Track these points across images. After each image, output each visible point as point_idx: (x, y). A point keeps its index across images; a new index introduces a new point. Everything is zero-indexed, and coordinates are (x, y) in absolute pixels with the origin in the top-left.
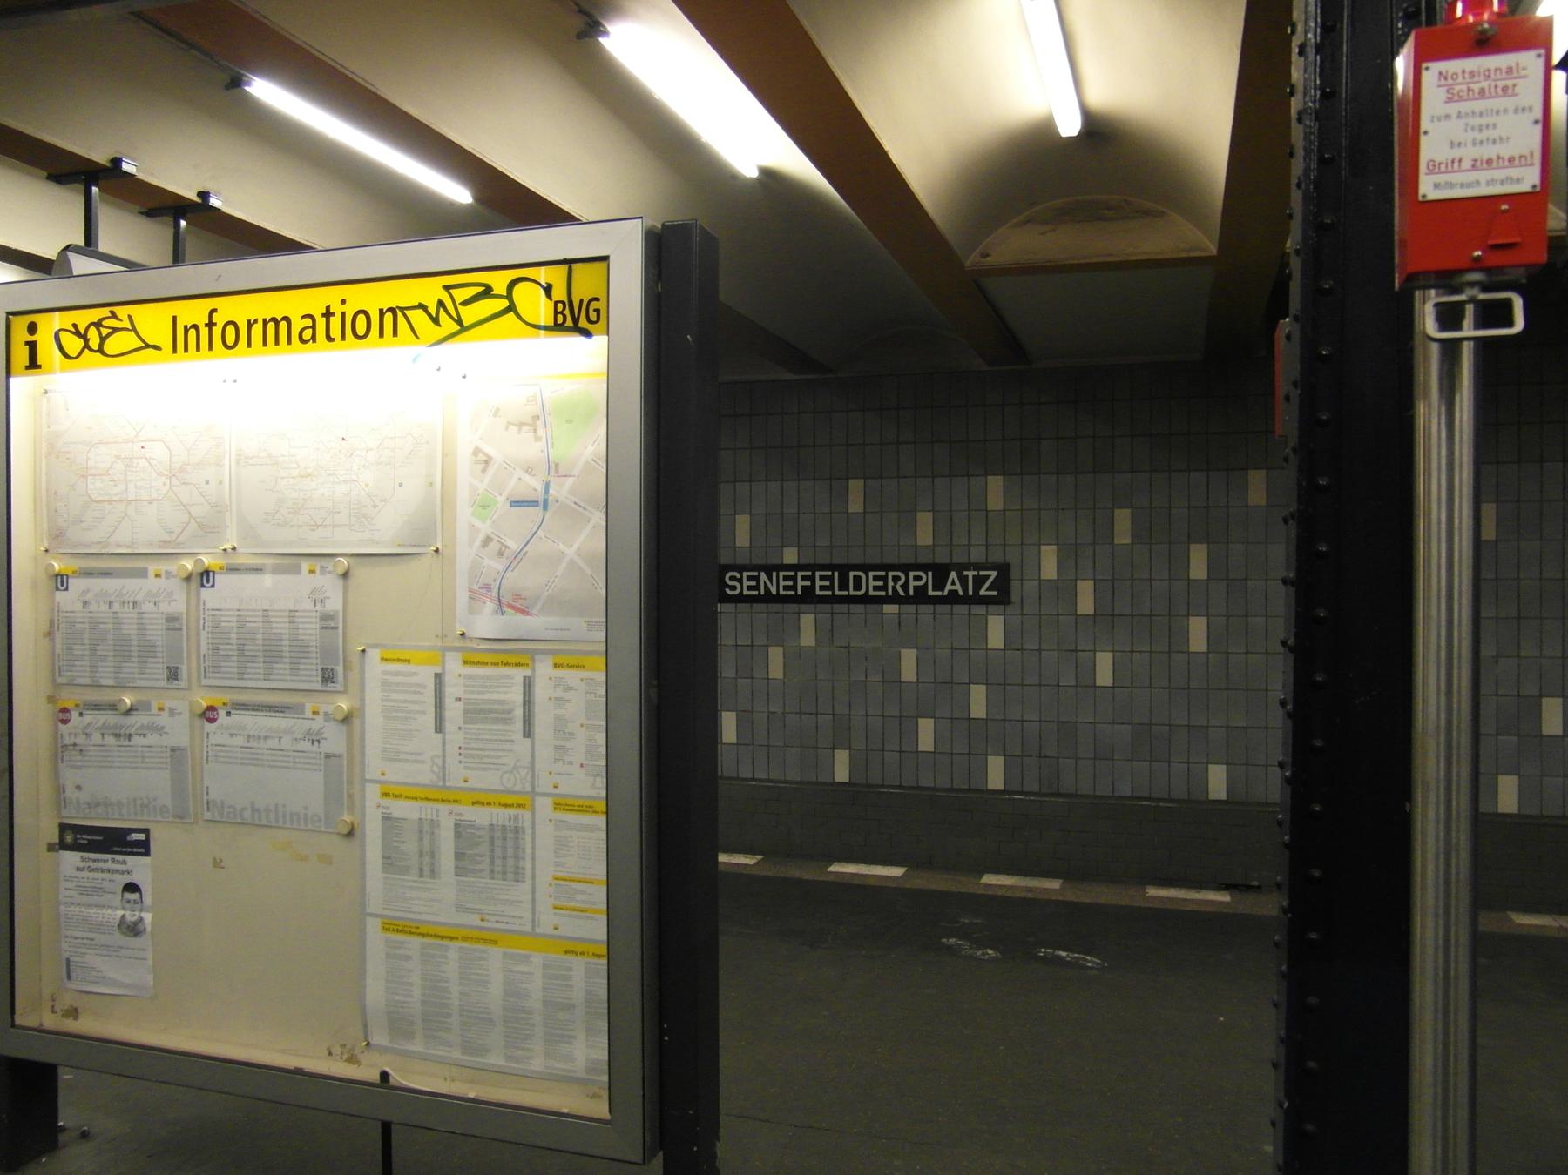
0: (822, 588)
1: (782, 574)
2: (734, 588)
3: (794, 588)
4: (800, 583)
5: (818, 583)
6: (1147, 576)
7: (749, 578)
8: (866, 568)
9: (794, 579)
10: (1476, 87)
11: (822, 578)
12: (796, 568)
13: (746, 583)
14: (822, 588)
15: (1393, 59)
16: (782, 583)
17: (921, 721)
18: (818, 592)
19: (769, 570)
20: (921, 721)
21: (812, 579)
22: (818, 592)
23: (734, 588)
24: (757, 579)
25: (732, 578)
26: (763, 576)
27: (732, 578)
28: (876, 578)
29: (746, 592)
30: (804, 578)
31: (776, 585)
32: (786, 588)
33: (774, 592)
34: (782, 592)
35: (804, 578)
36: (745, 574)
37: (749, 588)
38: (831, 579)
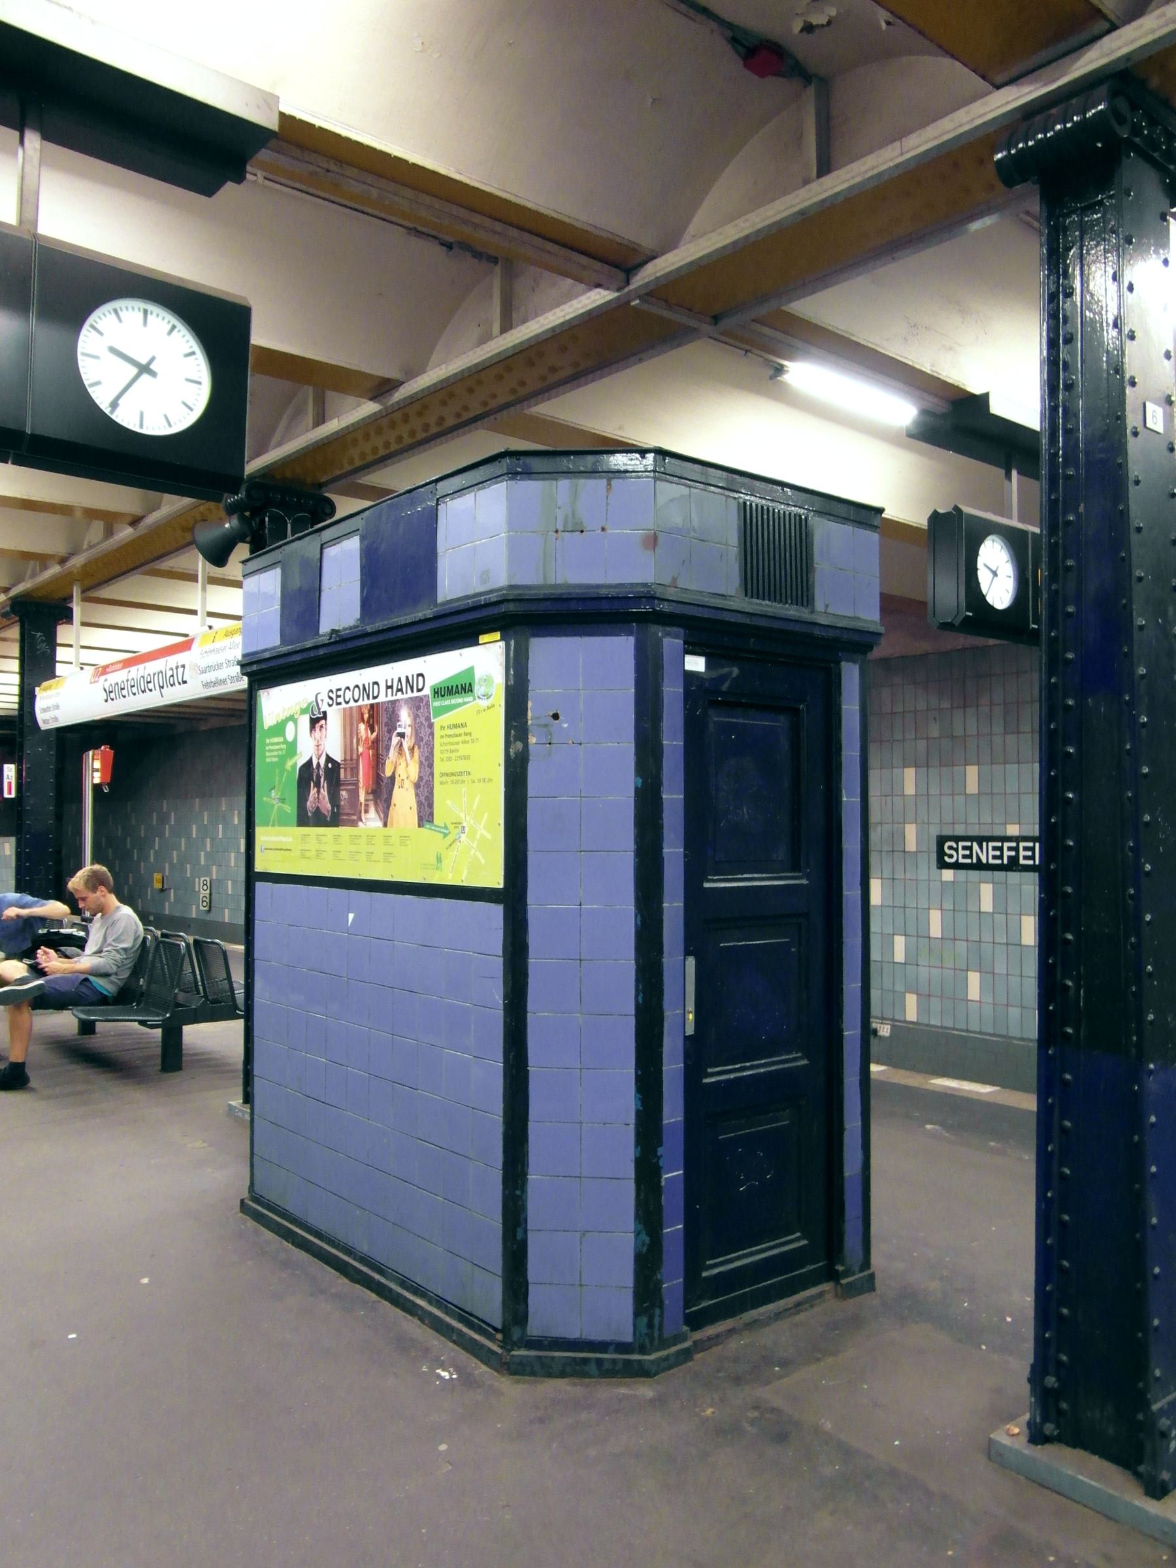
0: (1025, 858)
1: (991, 844)
2: (951, 856)
3: (1001, 857)
4: (1006, 853)
5: (1022, 853)
6: (1024, 887)
7: (964, 848)
8: (957, 839)
9: (1001, 849)
10: (431, 419)
11: (1025, 849)
12: (1018, 839)
13: (961, 852)
14: (1025, 858)
15: (651, 1240)
16: (991, 853)
17: (908, 995)
18: (1022, 862)
19: (980, 840)
20: (908, 995)
21: (1016, 849)
22: (1022, 862)
23: (951, 856)
24: (970, 848)
25: (950, 848)
26: (975, 846)
27: (950, 848)
28: (994, 849)
29: (961, 861)
30: (1010, 849)
31: (986, 854)
32: (994, 857)
33: (984, 861)
34: (991, 861)
35: (1010, 849)
36: (961, 844)
37: (964, 857)
38: (1032, 849)
